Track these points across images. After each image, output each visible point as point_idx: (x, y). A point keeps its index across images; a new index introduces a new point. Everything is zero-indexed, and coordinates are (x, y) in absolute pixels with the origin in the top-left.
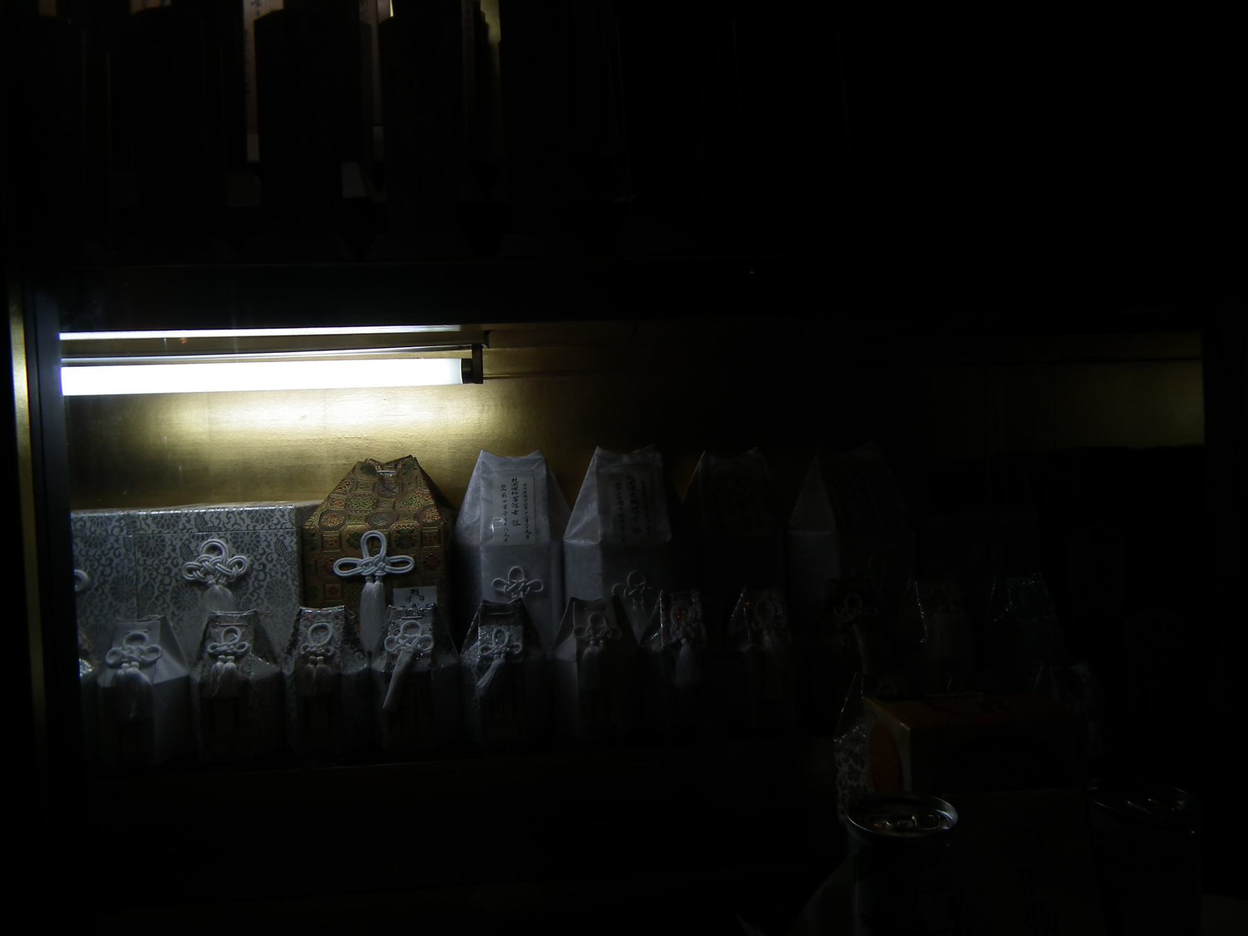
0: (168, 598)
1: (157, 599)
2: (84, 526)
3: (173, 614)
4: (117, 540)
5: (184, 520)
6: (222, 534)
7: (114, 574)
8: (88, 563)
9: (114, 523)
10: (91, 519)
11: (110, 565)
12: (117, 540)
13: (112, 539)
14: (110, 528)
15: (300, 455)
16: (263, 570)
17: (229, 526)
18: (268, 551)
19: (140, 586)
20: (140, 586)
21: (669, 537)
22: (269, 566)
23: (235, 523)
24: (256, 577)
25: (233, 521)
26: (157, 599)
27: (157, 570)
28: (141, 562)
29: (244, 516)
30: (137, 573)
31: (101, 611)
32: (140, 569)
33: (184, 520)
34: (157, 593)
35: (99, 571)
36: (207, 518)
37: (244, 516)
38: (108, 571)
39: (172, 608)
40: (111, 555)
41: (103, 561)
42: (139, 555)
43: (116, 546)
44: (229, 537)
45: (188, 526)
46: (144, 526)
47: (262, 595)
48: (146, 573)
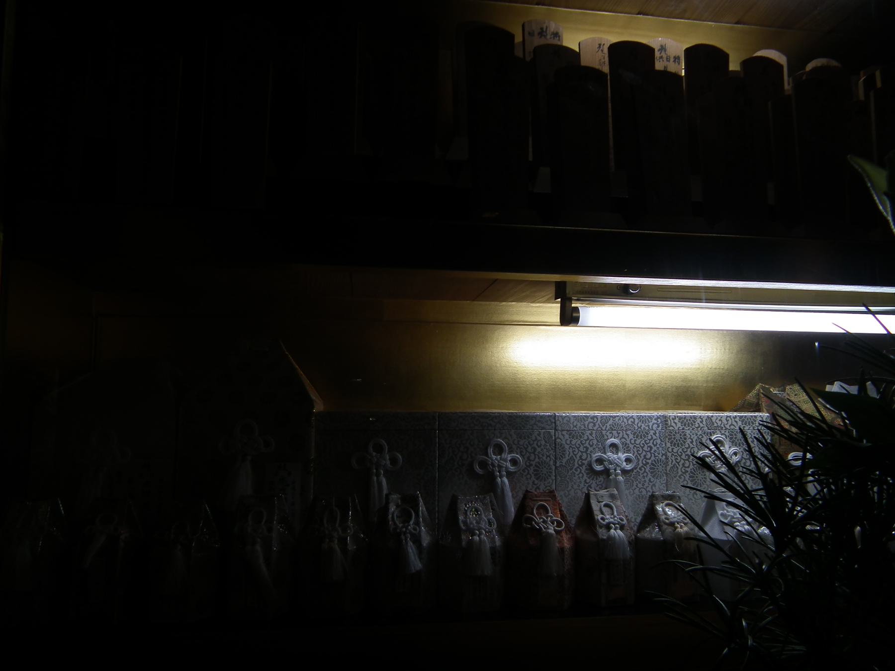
0: (531, 471)
1: (576, 470)
4: (655, 434)
5: (699, 420)
6: (723, 432)
8: (635, 450)
9: (590, 420)
10: (639, 417)
12: (655, 434)
14: (651, 424)
15: (685, 379)
17: (727, 426)
22: (654, 448)
23: (732, 425)
25: (730, 423)
26: (576, 470)
27: (526, 449)
28: (670, 450)
29: (737, 419)
30: (667, 458)
31: (643, 485)
32: (669, 454)
33: (699, 420)
34: (576, 465)
35: (642, 455)
36: (714, 419)
37: (737, 419)
41: (581, 449)
42: (669, 445)
44: (727, 434)
45: (701, 425)
46: (673, 424)
48: (571, 450)
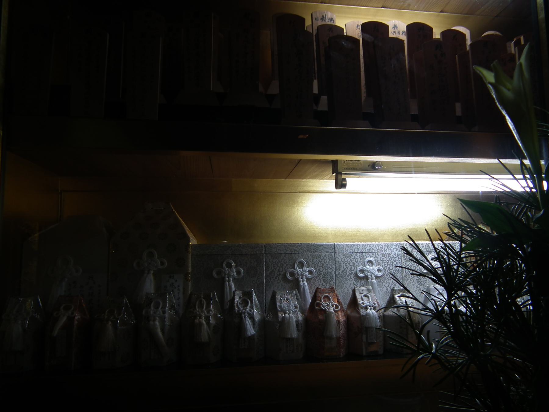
2: (343, 248)
3: (322, 284)
4: (395, 254)
7: (324, 271)
8: (383, 264)
10: (385, 245)
11: (322, 267)
12: (395, 254)
13: (393, 253)
16: (322, 267)
18: (395, 256)
19: (404, 274)
20: (404, 274)
21: (496, 60)
24: (279, 271)
26: (276, 278)
38: (321, 269)
39: (322, 282)
40: (354, 261)
42: (403, 261)
43: (395, 256)
47: (280, 278)
